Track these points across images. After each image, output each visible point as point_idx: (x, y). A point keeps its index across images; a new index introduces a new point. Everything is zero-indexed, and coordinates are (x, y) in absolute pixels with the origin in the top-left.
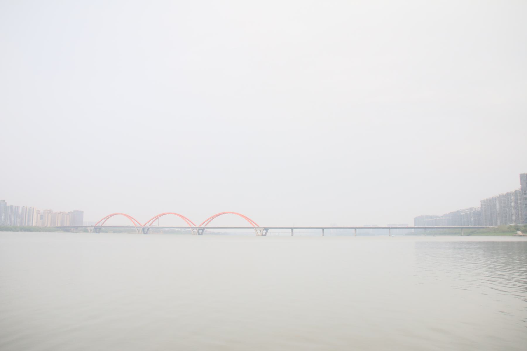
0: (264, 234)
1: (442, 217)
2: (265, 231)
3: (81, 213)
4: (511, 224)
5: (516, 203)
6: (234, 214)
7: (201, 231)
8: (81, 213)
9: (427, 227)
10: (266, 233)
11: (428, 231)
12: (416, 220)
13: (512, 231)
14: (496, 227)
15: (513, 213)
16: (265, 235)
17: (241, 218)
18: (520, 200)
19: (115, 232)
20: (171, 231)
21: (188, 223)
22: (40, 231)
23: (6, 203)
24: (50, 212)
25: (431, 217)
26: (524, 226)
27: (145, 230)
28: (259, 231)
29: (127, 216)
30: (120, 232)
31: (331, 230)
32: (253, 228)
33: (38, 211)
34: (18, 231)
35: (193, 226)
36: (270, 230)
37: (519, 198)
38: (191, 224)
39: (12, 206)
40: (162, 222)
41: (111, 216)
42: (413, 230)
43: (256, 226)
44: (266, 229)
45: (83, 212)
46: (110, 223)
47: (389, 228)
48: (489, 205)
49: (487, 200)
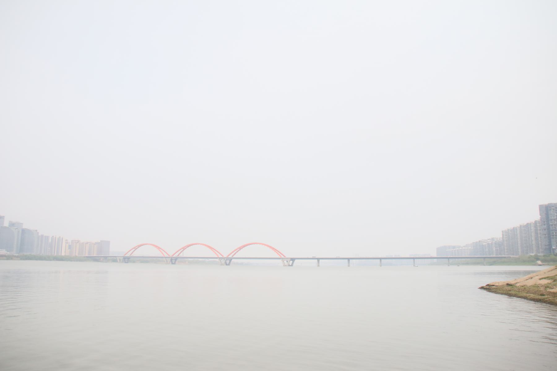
0: (290, 264)
1: (464, 247)
2: (291, 262)
4: (531, 254)
5: (536, 233)
7: (228, 261)
8: (108, 243)
9: (449, 258)
10: (293, 263)
11: (451, 260)
13: (532, 261)
14: (517, 257)
15: (534, 243)
16: (292, 265)
17: (268, 248)
18: (540, 230)
19: (142, 262)
20: (145, 260)
22: (71, 261)
23: (38, 233)
24: (78, 241)
25: (454, 247)
26: (544, 256)
27: (174, 260)
28: (285, 262)
29: (156, 246)
30: (147, 262)
31: (354, 260)
32: (280, 258)
33: (66, 240)
34: (51, 260)
35: (220, 256)
36: (296, 261)
37: (538, 228)
39: (42, 236)
40: (138, 253)
41: (244, 246)
42: (435, 260)
43: (283, 257)
44: (293, 260)
47: (414, 258)
48: (510, 235)
49: (508, 230)
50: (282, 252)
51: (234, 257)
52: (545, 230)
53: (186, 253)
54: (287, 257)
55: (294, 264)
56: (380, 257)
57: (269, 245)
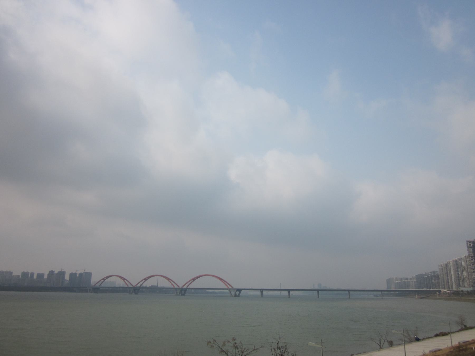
1: (411, 279)
3: (89, 275)
6: (212, 277)
8: (89, 275)
12: (389, 282)
16: (239, 296)
20: (154, 290)
21: (226, 285)
25: (401, 279)
36: (242, 291)
38: (128, 283)
43: (230, 287)
44: (240, 290)
45: (50, 272)
46: (148, 284)
50: (230, 283)
51: (190, 287)
52: (473, 264)
53: (195, 285)
54: (235, 288)
55: (241, 294)
56: (261, 288)
57: (214, 275)
